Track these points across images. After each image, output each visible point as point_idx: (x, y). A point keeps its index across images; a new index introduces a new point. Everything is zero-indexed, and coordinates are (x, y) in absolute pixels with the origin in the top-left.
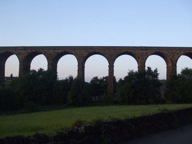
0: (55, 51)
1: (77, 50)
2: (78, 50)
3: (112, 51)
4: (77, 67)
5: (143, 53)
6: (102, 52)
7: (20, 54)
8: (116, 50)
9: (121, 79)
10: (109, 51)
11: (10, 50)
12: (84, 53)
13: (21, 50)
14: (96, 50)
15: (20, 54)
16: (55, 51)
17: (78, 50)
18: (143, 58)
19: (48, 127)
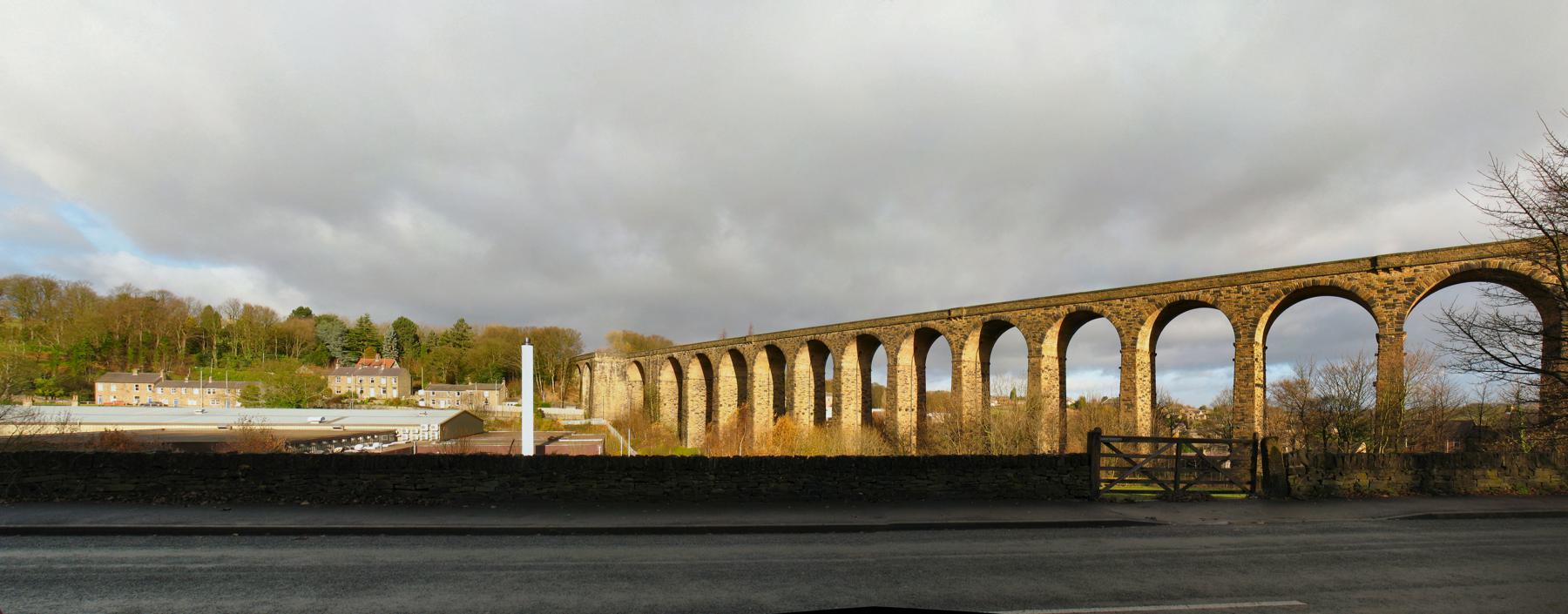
0: (1050, 312)
1: (1118, 301)
2: (1122, 300)
3: (1246, 288)
4: (991, 362)
5: (1390, 282)
6: (1209, 298)
7: (954, 331)
8: (1266, 285)
9: (1094, 400)
10: (1234, 289)
11: (929, 322)
12: (1143, 308)
13: (1502, 296)
14: (1185, 295)
15: (954, 331)
16: (1050, 312)
17: (1122, 300)
18: (1390, 301)
19: (136, 397)
